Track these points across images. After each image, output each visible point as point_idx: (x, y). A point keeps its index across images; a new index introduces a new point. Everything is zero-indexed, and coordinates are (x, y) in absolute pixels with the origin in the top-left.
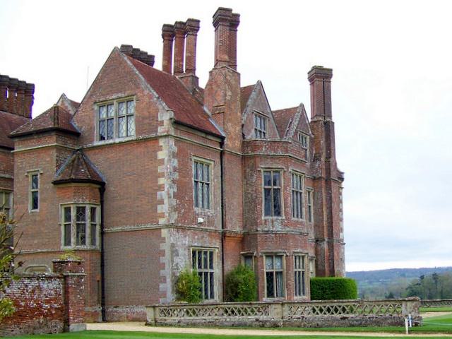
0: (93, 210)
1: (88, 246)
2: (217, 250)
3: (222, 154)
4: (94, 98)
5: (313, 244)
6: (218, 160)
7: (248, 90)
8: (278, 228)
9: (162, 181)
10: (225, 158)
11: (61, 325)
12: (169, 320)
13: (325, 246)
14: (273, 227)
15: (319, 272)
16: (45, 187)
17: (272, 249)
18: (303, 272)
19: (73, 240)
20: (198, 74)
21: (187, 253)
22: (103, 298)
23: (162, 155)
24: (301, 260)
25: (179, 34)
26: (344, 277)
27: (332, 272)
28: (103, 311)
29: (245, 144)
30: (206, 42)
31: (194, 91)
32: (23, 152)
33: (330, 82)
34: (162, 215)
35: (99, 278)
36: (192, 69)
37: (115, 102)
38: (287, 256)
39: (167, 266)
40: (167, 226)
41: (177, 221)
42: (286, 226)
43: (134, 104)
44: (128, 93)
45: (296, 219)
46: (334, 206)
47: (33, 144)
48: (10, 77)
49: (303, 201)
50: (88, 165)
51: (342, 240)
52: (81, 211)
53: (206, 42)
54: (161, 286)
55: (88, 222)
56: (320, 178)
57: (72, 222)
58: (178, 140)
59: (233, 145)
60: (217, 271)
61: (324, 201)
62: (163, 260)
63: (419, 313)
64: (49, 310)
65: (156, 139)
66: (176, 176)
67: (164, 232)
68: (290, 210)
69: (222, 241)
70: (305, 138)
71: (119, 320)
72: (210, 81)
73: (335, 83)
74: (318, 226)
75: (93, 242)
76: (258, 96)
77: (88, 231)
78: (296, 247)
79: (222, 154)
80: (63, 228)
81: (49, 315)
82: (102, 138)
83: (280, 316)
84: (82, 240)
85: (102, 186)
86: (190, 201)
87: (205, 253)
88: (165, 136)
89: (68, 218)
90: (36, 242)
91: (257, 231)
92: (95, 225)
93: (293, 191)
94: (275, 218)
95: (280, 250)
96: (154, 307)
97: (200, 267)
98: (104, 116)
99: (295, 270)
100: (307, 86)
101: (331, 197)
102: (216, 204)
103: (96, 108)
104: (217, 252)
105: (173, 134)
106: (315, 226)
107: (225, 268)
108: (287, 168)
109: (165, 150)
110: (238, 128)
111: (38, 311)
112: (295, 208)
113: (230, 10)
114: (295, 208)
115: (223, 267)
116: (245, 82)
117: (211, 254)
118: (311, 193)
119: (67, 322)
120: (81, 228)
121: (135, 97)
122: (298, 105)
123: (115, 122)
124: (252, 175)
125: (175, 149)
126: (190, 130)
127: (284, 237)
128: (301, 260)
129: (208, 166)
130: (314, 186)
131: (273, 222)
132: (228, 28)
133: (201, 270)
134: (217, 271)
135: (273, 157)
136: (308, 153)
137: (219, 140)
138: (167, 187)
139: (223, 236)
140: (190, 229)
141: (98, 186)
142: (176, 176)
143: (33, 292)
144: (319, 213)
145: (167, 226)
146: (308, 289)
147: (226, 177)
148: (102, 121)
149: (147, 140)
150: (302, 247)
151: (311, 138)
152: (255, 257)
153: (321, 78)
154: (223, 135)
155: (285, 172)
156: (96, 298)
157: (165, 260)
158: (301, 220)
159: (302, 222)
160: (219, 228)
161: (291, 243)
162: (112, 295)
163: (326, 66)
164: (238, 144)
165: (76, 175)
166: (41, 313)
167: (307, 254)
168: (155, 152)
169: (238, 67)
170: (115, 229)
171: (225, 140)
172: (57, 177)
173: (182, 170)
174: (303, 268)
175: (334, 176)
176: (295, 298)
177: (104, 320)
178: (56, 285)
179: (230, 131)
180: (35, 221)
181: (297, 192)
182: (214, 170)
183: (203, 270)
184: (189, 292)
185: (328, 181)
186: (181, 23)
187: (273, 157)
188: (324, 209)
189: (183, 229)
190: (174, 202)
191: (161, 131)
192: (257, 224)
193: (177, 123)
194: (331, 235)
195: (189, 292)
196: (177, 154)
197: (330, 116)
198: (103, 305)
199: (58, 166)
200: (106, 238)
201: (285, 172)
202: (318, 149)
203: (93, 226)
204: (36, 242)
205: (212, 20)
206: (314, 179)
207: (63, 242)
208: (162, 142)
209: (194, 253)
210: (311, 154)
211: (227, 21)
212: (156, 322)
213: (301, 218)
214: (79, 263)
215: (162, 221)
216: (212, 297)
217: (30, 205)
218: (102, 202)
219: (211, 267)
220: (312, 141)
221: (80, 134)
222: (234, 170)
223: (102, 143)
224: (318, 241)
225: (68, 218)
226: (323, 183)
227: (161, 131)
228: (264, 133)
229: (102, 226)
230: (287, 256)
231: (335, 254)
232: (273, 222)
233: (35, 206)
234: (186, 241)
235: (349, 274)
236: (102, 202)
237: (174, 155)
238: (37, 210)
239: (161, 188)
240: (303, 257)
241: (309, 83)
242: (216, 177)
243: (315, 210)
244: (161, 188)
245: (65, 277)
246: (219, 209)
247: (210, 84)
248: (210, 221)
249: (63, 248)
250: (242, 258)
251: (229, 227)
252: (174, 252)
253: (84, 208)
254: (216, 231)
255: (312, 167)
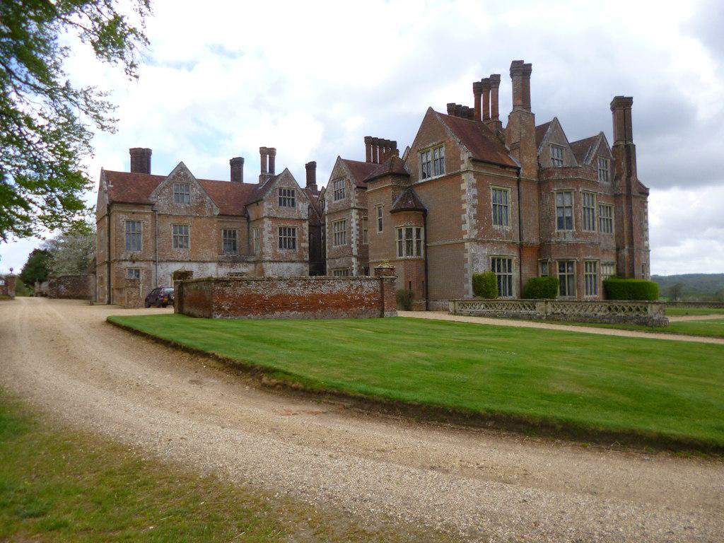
0: (418, 231)
1: (414, 257)
2: (515, 258)
3: (519, 181)
4: (418, 148)
5: (614, 252)
6: (515, 187)
7: (544, 128)
8: (570, 239)
9: (464, 206)
10: (522, 185)
11: (379, 312)
12: (464, 311)
13: (625, 253)
14: (565, 238)
15: (619, 274)
16: (386, 216)
17: (563, 256)
18: (595, 276)
19: (404, 252)
20: (500, 118)
21: (486, 261)
22: (427, 293)
23: (464, 186)
24: (593, 266)
25: (486, 88)
26: (649, 280)
27: (632, 275)
28: (427, 304)
29: (541, 171)
30: (506, 89)
31: (498, 134)
32: (372, 192)
33: (631, 109)
34: (465, 232)
35: (423, 279)
36: (496, 115)
37: (431, 149)
38: (577, 262)
39: (469, 271)
40: (469, 240)
41: (477, 236)
42: (577, 237)
43: (444, 149)
44: (440, 141)
45: (586, 231)
46: (635, 218)
47: (378, 186)
48: (268, 147)
49: (596, 215)
50: (414, 198)
51: (647, 247)
52: (409, 231)
53: (506, 89)
54: (465, 286)
55: (414, 239)
56: (622, 194)
57: (403, 240)
58: (476, 175)
59: (529, 173)
60: (515, 274)
61: (625, 214)
62: (466, 266)
63: (665, 314)
64: (369, 302)
65: (459, 174)
66: (476, 201)
67: (467, 245)
68: (581, 224)
69: (520, 250)
70: (606, 162)
71: (437, 310)
72: (509, 123)
73: (635, 109)
74: (619, 236)
75: (418, 253)
76: (553, 131)
77: (415, 245)
78: (587, 254)
79: (519, 181)
80: (397, 243)
81: (369, 305)
82: (424, 176)
83: (544, 312)
84: (409, 251)
85: (425, 213)
86: (489, 220)
87: (504, 260)
88: (467, 171)
89: (400, 237)
90: (382, 254)
91: (550, 241)
92: (420, 241)
93: (584, 208)
94: (566, 231)
95: (571, 257)
96: (454, 301)
97: (499, 271)
98: (424, 161)
99: (585, 273)
100: (610, 114)
101: (631, 211)
102: (514, 222)
103: (419, 154)
104: (515, 259)
105: (472, 169)
106: (616, 236)
107: (523, 272)
108: (578, 188)
109: (468, 181)
110: (534, 160)
111: (360, 302)
112: (587, 222)
113: (523, 61)
114: (587, 222)
115: (520, 271)
116: (539, 122)
117: (510, 261)
118: (613, 209)
119: (383, 311)
120: (409, 243)
121: (444, 144)
122: (597, 134)
123: (432, 165)
124: (546, 197)
125: (475, 181)
126: (488, 165)
127: (575, 246)
128: (593, 266)
129: (506, 191)
130: (615, 202)
131: (564, 234)
132: (521, 77)
133: (500, 274)
134: (515, 274)
135: (564, 181)
136: (609, 174)
137: (515, 171)
138: (468, 211)
139: (521, 248)
140: (488, 242)
141: (422, 213)
142: (476, 201)
143: (357, 289)
144: (619, 225)
145: (469, 240)
146: (600, 289)
147: (523, 200)
148: (423, 164)
149: (455, 176)
150: (593, 255)
151: (611, 161)
152: (550, 263)
153: (622, 106)
154: (519, 166)
155: (575, 192)
156: (421, 294)
157: (466, 266)
158: (593, 231)
159: (593, 234)
160: (517, 240)
161: (581, 251)
162: (434, 292)
163: (626, 95)
164: (534, 172)
165: (405, 205)
166: (363, 304)
167: (599, 260)
168: (460, 184)
169: (532, 109)
170: (435, 244)
171: (521, 170)
172: (392, 207)
173: (482, 196)
174: (595, 271)
175: (635, 191)
176: (585, 297)
177: (427, 310)
178: (374, 284)
179: (526, 163)
180: (381, 239)
181: (589, 209)
182: (511, 194)
183: (589, 273)
184: (484, 289)
185: (629, 197)
186: (486, 79)
187: (564, 181)
188: (625, 221)
189: (483, 242)
190: (474, 222)
191: (463, 167)
192: (550, 236)
193: (474, 161)
194: (631, 244)
195: (484, 289)
196: (476, 184)
197: (631, 140)
198: (427, 299)
199: (394, 200)
200: (428, 250)
201: (575, 192)
202: (619, 169)
203: (418, 242)
204: (382, 254)
205: (509, 73)
206: (615, 196)
207: (398, 253)
208: (463, 177)
209: (493, 260)
210: (612, 174)
211: (521, 71)
212: (455, 311)
213: (594, 229)
214: (392, 269)
215: (465, 237)
216: (510, 294)
217: (378, 229)
218: (425, 225)
219: (510, 271)
220: (613, 163)
221: (409, 175)
222: (530, 194)
223: (424, 180)
224: (618, 249)
225: (400, 237)
226: (624, 199)
227: (463, 167)
228: (562, 161)
229: (426, 242)
230: (577, 262)
231: (636, 259)
232: (564, 234)
233: (381, 229)
234: (486, 251)
235: (656, 278)
236: (425, 225)
237: (474, 186)
238: (382, 232)
239: (464, 211)
240: (595, 263)
241: (612, 112)
242: (513, 200)
243: (616, 222)
244: (464, 211)
245: (382, 279)
246: (517, 225)
247: (508, 126)
248: (509, 235)
249: (398, 258)
250: (539, 263)
251: (526, 239)
252: (475, 260)
253: (411, 229)
254: (513, 243)
255: (613, 186)
